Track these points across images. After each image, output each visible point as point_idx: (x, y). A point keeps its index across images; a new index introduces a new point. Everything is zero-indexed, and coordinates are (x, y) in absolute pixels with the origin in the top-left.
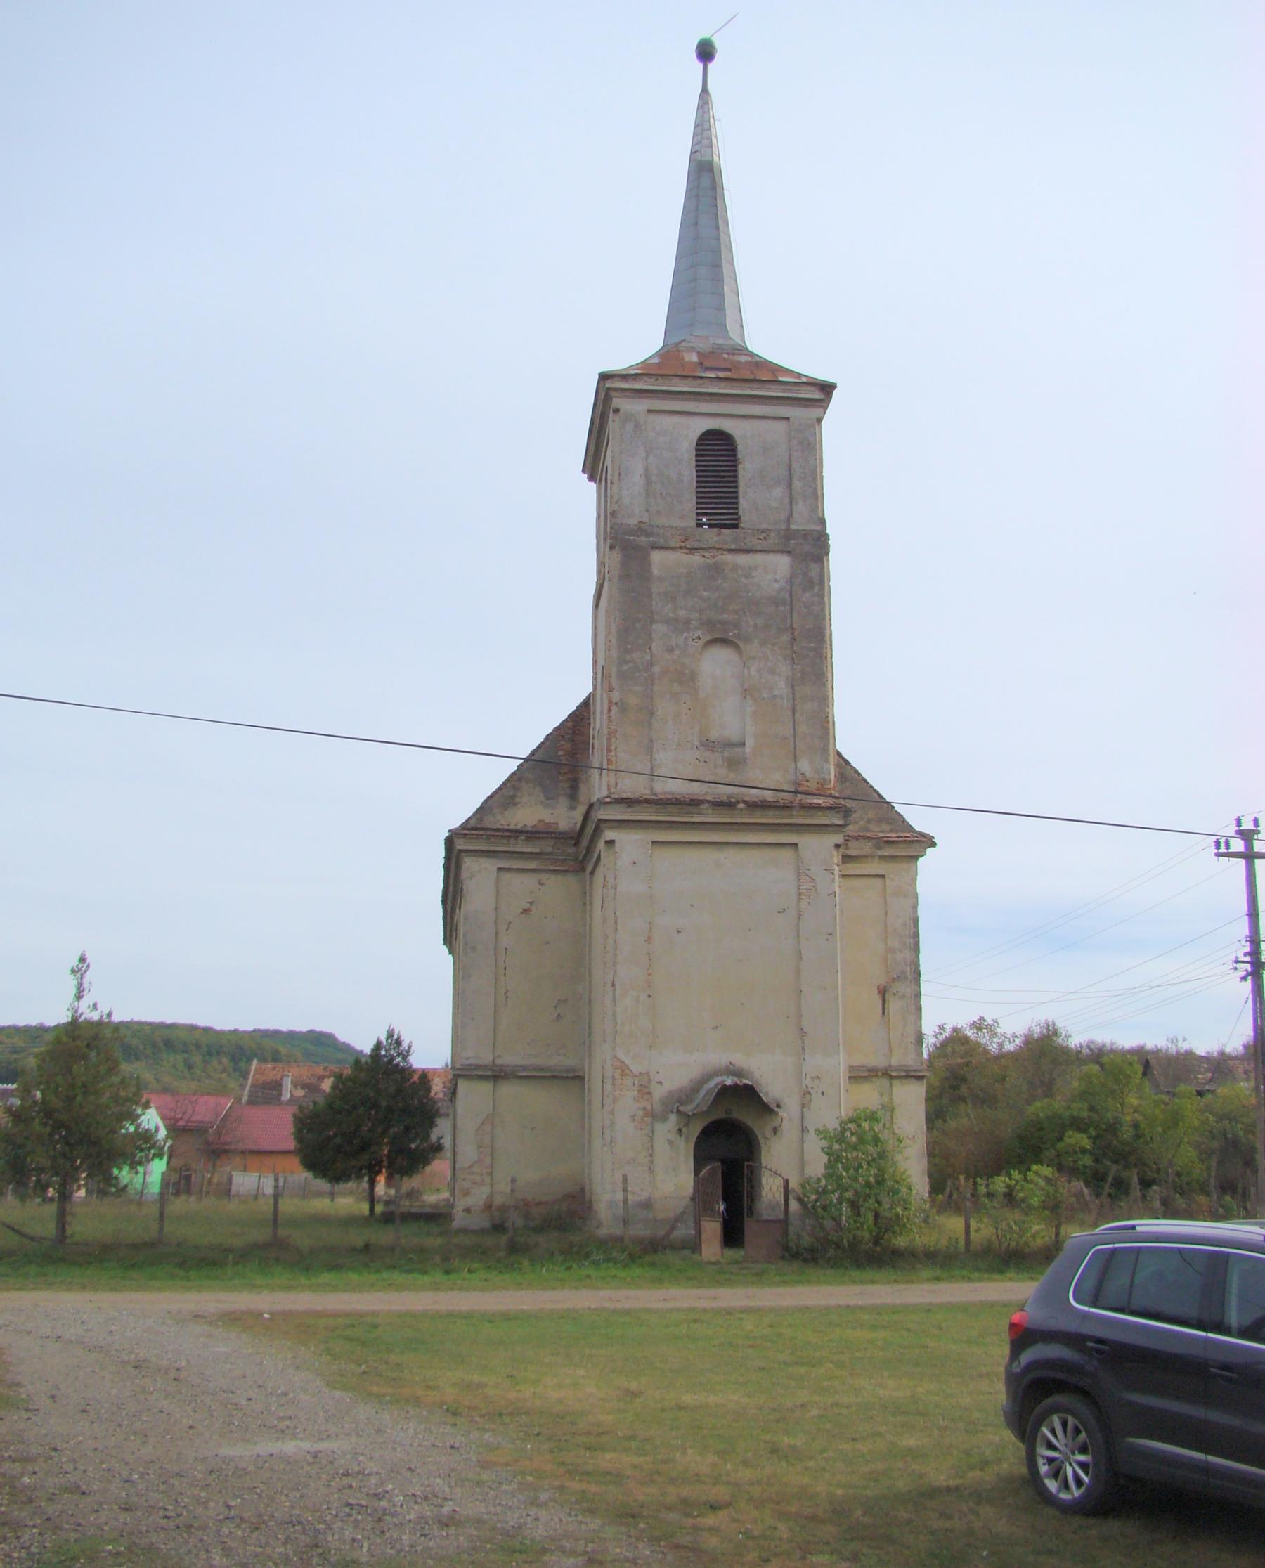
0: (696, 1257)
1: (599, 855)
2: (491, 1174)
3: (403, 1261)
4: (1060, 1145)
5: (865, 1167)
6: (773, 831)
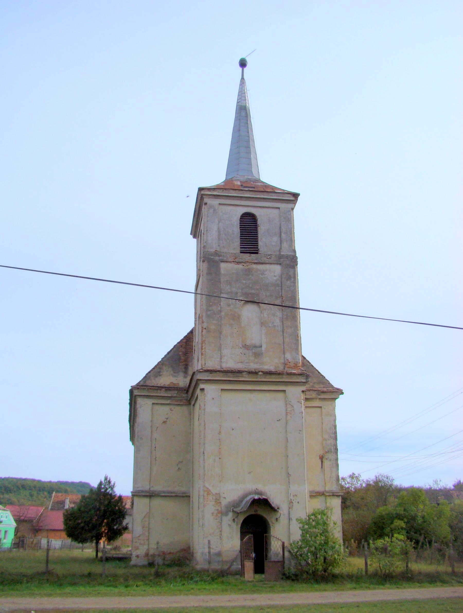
0: (242, 578)
1: (197, 395)
2: (148, 539)
3: (106, 581)
4: (392, 526)
5: (319, 536)
6: (276, 385)
